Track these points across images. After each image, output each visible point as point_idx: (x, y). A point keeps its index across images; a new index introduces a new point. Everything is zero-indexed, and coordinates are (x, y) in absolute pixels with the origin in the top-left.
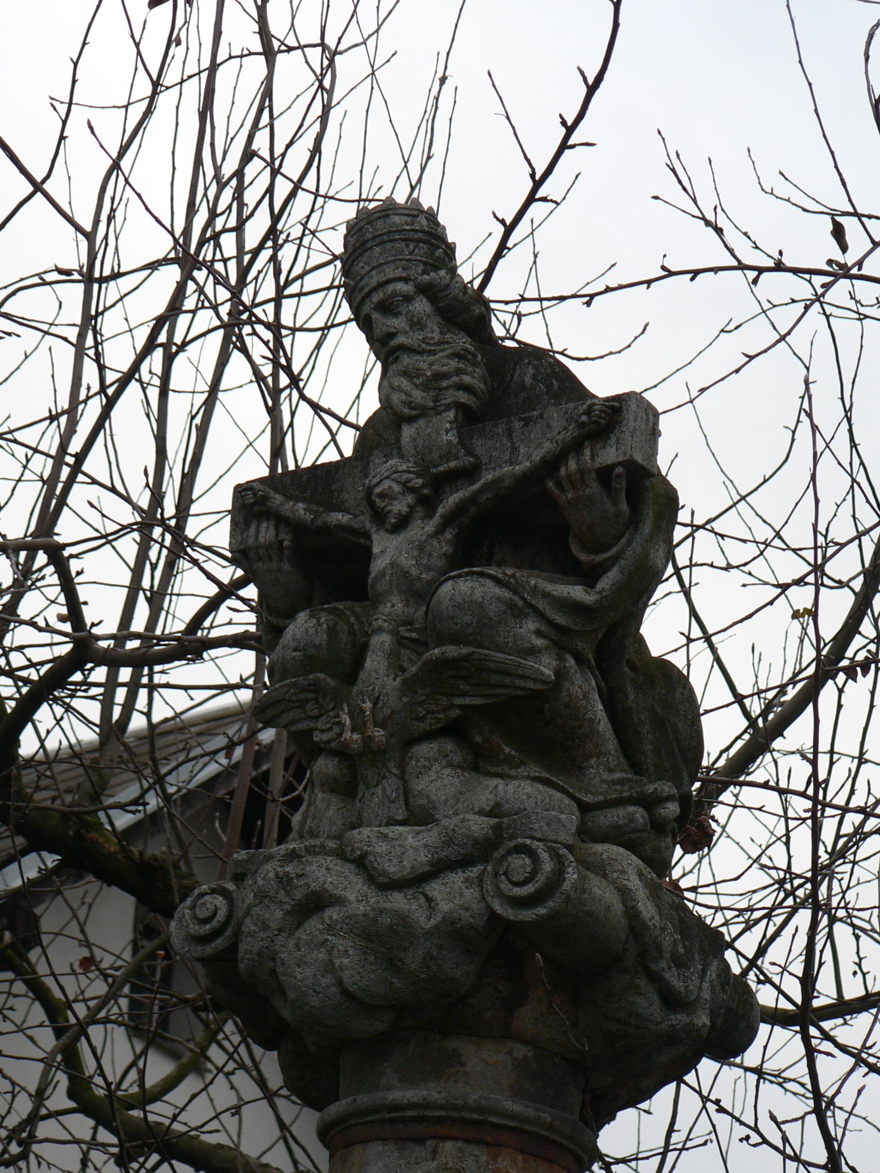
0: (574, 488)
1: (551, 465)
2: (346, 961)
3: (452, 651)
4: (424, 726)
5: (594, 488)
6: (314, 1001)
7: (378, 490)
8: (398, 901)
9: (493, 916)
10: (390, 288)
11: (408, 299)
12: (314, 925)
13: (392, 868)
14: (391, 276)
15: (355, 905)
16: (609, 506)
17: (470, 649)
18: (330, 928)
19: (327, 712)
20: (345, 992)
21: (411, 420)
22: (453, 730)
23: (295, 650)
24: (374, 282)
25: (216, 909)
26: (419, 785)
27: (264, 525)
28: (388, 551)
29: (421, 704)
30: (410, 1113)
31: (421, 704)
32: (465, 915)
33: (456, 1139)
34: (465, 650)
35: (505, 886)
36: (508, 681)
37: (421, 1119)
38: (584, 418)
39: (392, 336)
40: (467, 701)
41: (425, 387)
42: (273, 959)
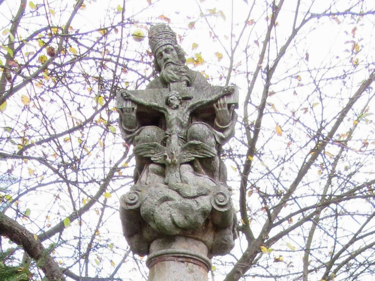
0: (221, 108)
1: (216, 101)
2: (175, 215)
3: (197, 142)
4: (185, 160)
5: (226, 108)
6: (166, 224)
7: (171, 98)
8: (189, 202)
9: (213, 208)
10: (168, 46)
11: (172, 50)
12: (165, 204)
13: (188, 193)
14: (168, 43)
15: (177, 201)
16: (229, 114)
17: (201, 143)
18: (170, 206)
19: (157, 153)
20: (174, 222)
21: (173, 82)
22: (191, 163)
23: (149, 135)
24: (164, 43)
25: (135, 197)
26: (184, 175)
27: (128, 103)
28: (172, 115)
29: (185, 154)
30: (182, 255)
31: (185, 154)
32: (207, 208)
33: (192, 263)
34: (201, 143)
35: (217, 202)
36: (208, 152)
37: (184, 257)
38: (226, 90)
39: (168, 59)
40: (197, 156)
41: (177, 74)
42: (153, 212)
